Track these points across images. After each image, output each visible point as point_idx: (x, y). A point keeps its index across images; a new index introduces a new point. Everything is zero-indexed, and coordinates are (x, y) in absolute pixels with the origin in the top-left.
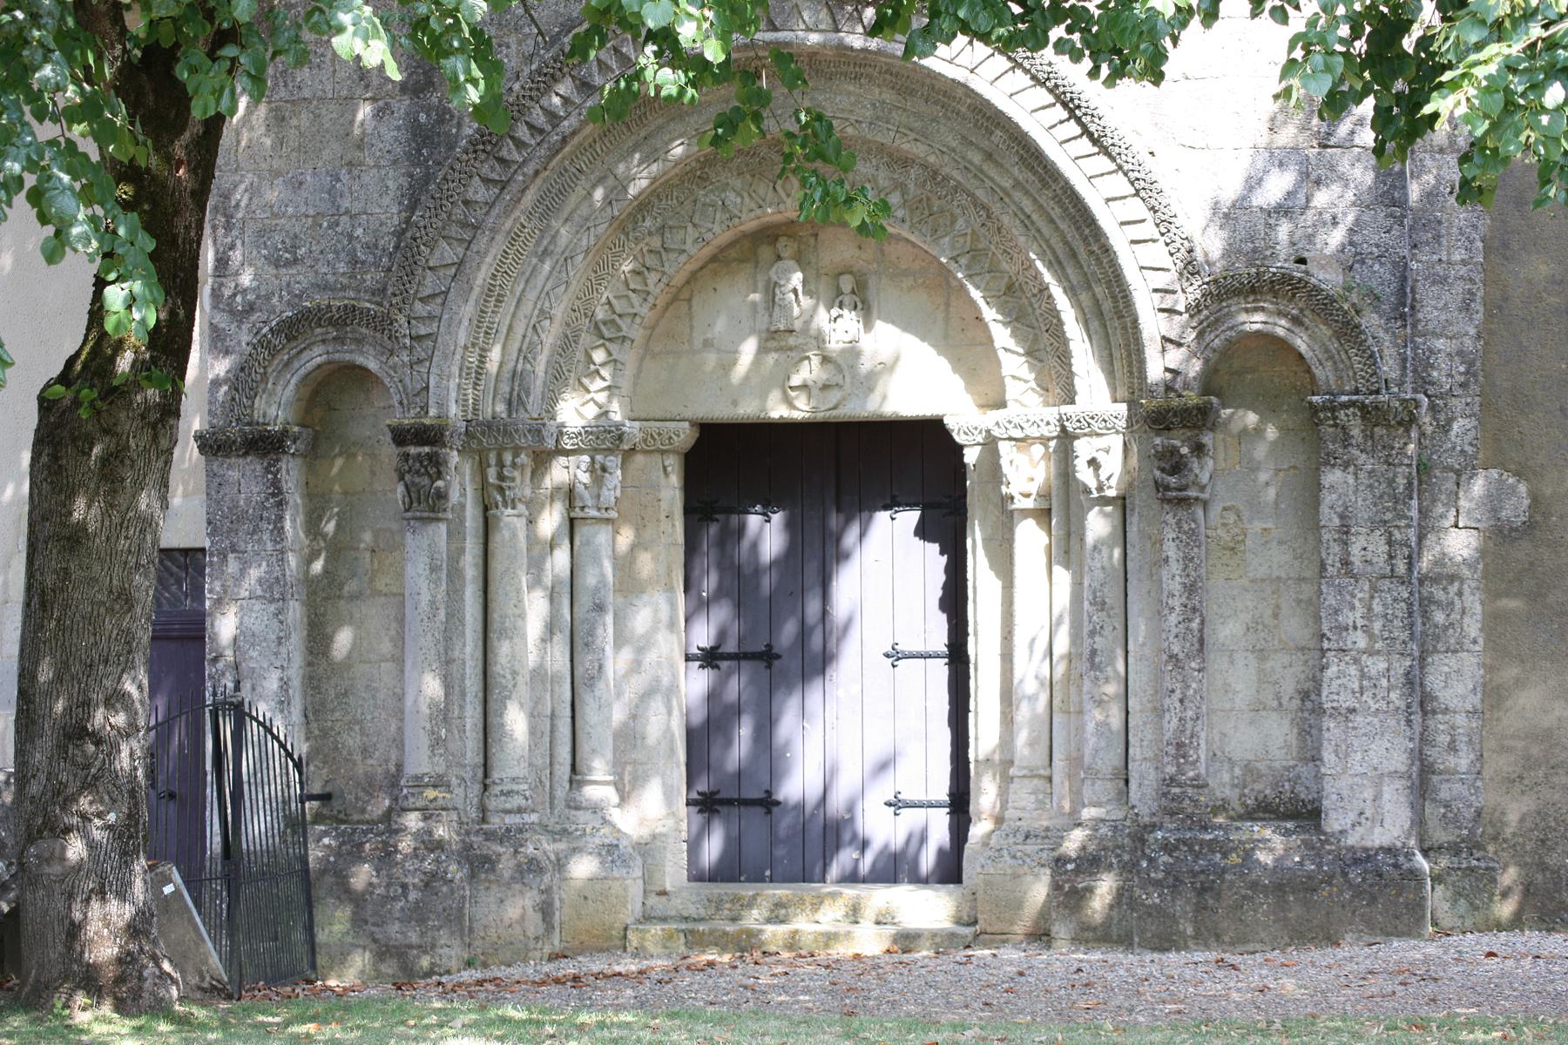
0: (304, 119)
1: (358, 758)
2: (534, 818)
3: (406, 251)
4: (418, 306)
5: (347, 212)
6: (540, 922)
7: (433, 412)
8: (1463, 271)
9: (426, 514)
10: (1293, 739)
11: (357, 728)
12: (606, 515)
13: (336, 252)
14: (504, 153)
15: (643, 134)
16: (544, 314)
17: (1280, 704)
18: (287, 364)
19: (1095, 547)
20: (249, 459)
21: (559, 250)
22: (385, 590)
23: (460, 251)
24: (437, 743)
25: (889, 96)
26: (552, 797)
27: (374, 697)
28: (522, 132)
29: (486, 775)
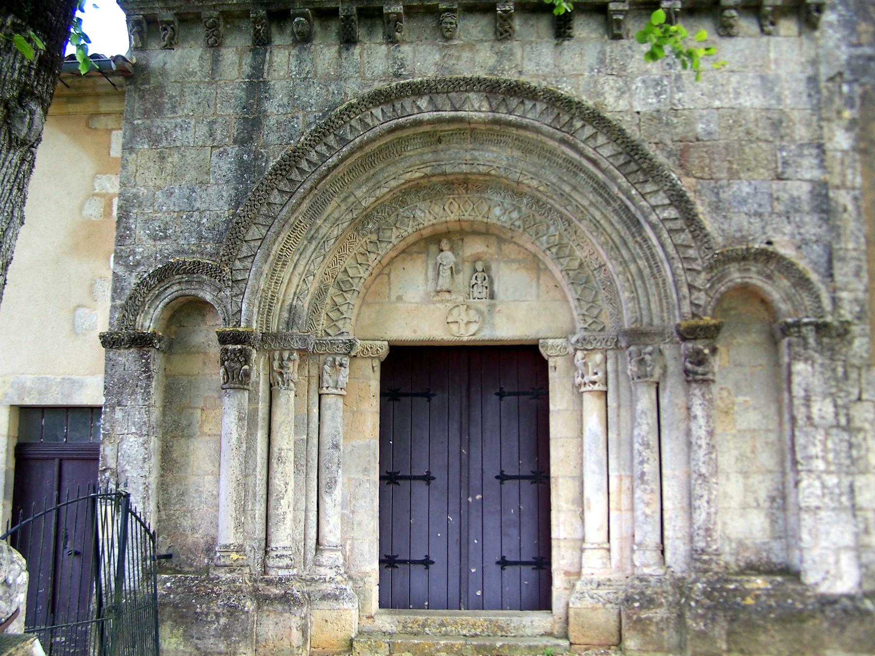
0: (176, 158)
2: (295, 571)
3: (232, 234)
4: (237, 263)
5: (198, 209)
6: (301, 637)
7: (243, 324)
8: (854, 254)
9: (237, 386)
10: (766, 524)
11: (189, 515)
12: (341, 393)
13: (190, 232)
14: (293, 177)
15: (372, 172)
17: (758, 505)
18: (157, 296)
19: (642, 412)
20: (132, 350)
21: (320, 236)
23: (264, 232)
24: (239, 525)
25: (517, 153)
26: (305, 559)
27: (200, 497)
28: (304, 165)
29: (267, 545)
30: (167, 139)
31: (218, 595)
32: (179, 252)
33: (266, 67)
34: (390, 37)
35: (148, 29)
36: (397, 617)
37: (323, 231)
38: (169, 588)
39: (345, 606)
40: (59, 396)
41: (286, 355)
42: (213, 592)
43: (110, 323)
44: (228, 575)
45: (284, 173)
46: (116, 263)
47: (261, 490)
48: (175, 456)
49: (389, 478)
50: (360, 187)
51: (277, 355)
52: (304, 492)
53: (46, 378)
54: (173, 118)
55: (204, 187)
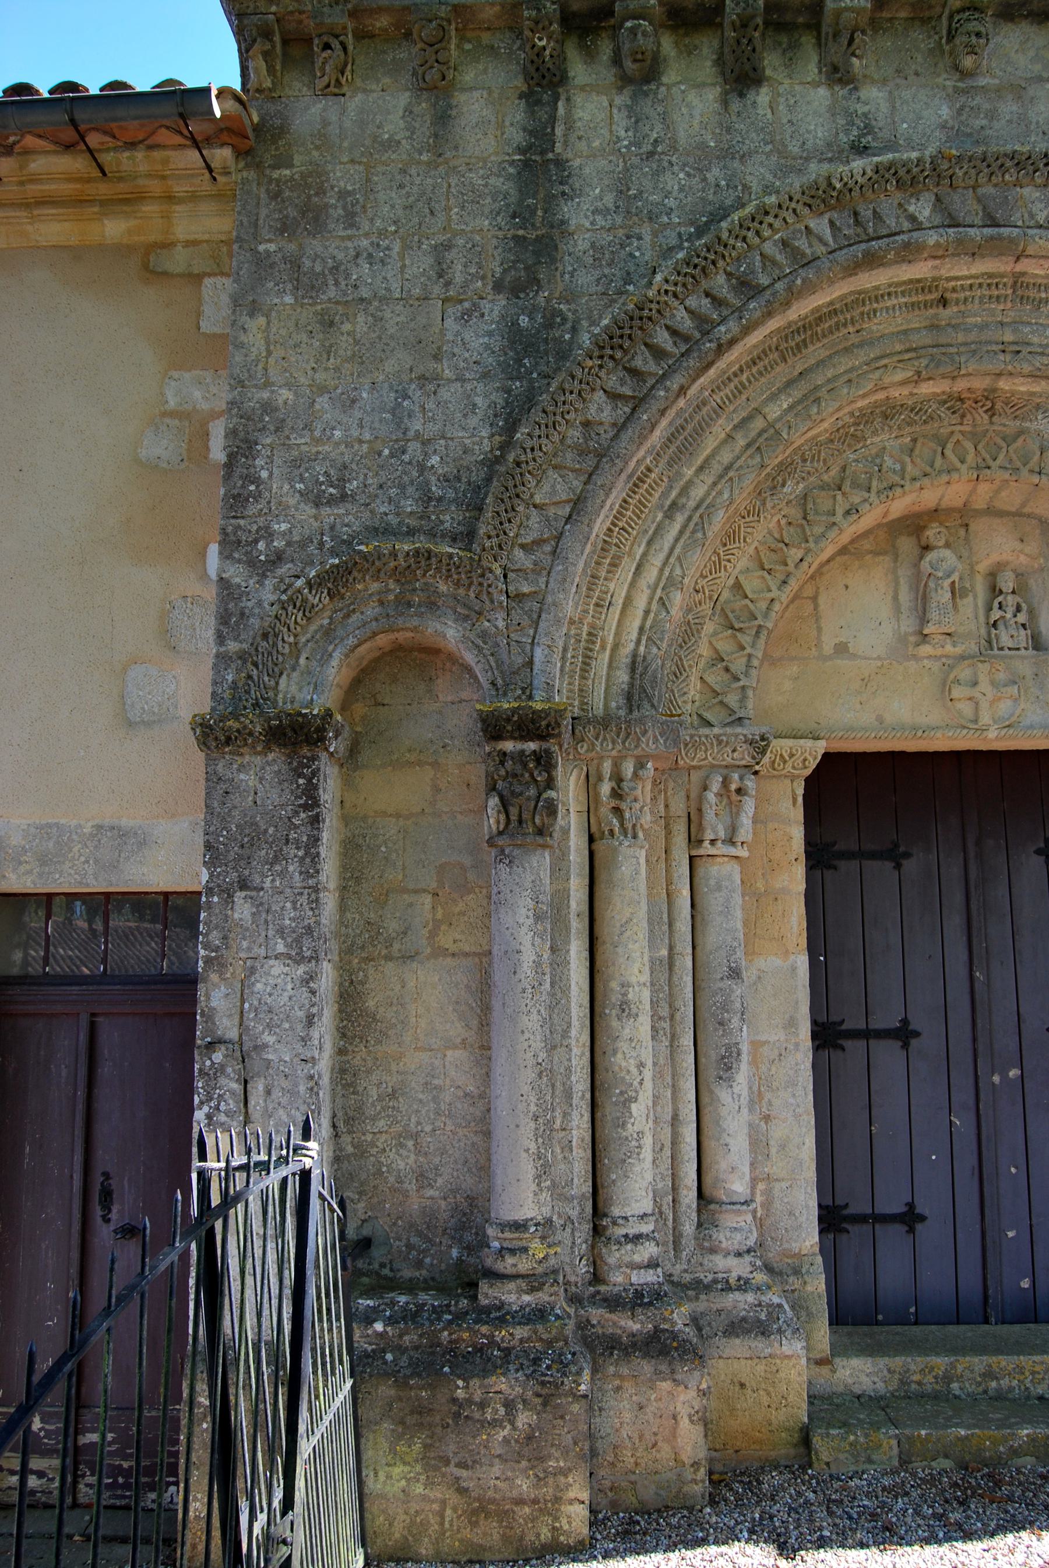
1: (411, 1187)
4: (519, 554)
5: (418, 435)
7: (538, 695)
13: (402, 487)
14: (638, 363)
15: (799, 368)
16: (671, 583)
20: (271, 756)
21: (692, 504)
22: (453, 948)
23: (577, 484)
27: (435, 1099)
28: (662, 338)
29: (598, 1212)
30: (337, 283)
31: (507, 1352)
32: (375, 531)
33: (559, 131)
34: (835, 69)
35: (285, 54)
36: (886, 1360)
37: (698, 492)
38: (381, 1335)
39: (786, 1349)
40: (90, 869)
41: (628, 769)
42: (492, 1343)
43: (214, 694)
44: (527, 1298)
45: (619, 354)
46: (226, 555)
47: (580, 1083)
48: (371, 1003)
49: (826, 1036)
50: (773, 397)
51: (607, 767)
52: (669, 1079)
53: (57, 824)
54: (350, 238)
55: (431, 387)
